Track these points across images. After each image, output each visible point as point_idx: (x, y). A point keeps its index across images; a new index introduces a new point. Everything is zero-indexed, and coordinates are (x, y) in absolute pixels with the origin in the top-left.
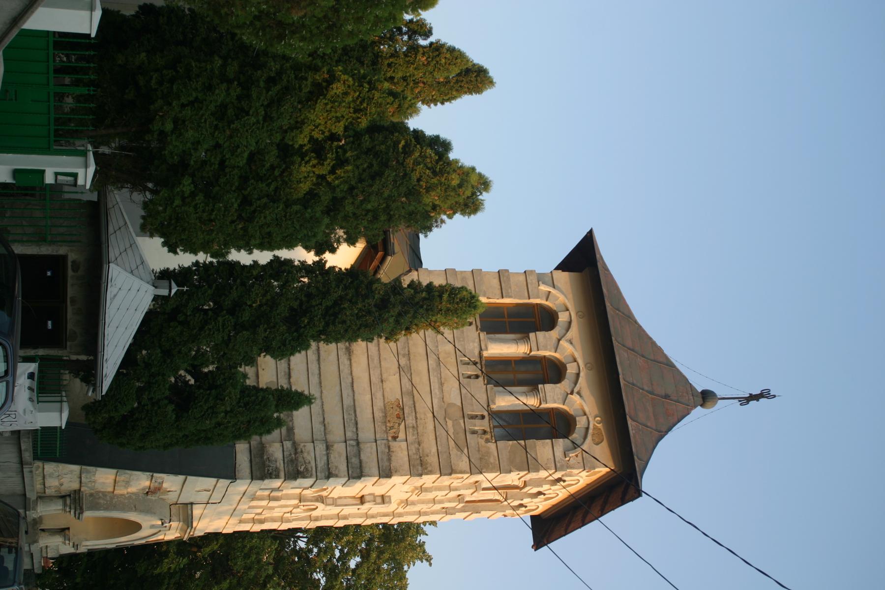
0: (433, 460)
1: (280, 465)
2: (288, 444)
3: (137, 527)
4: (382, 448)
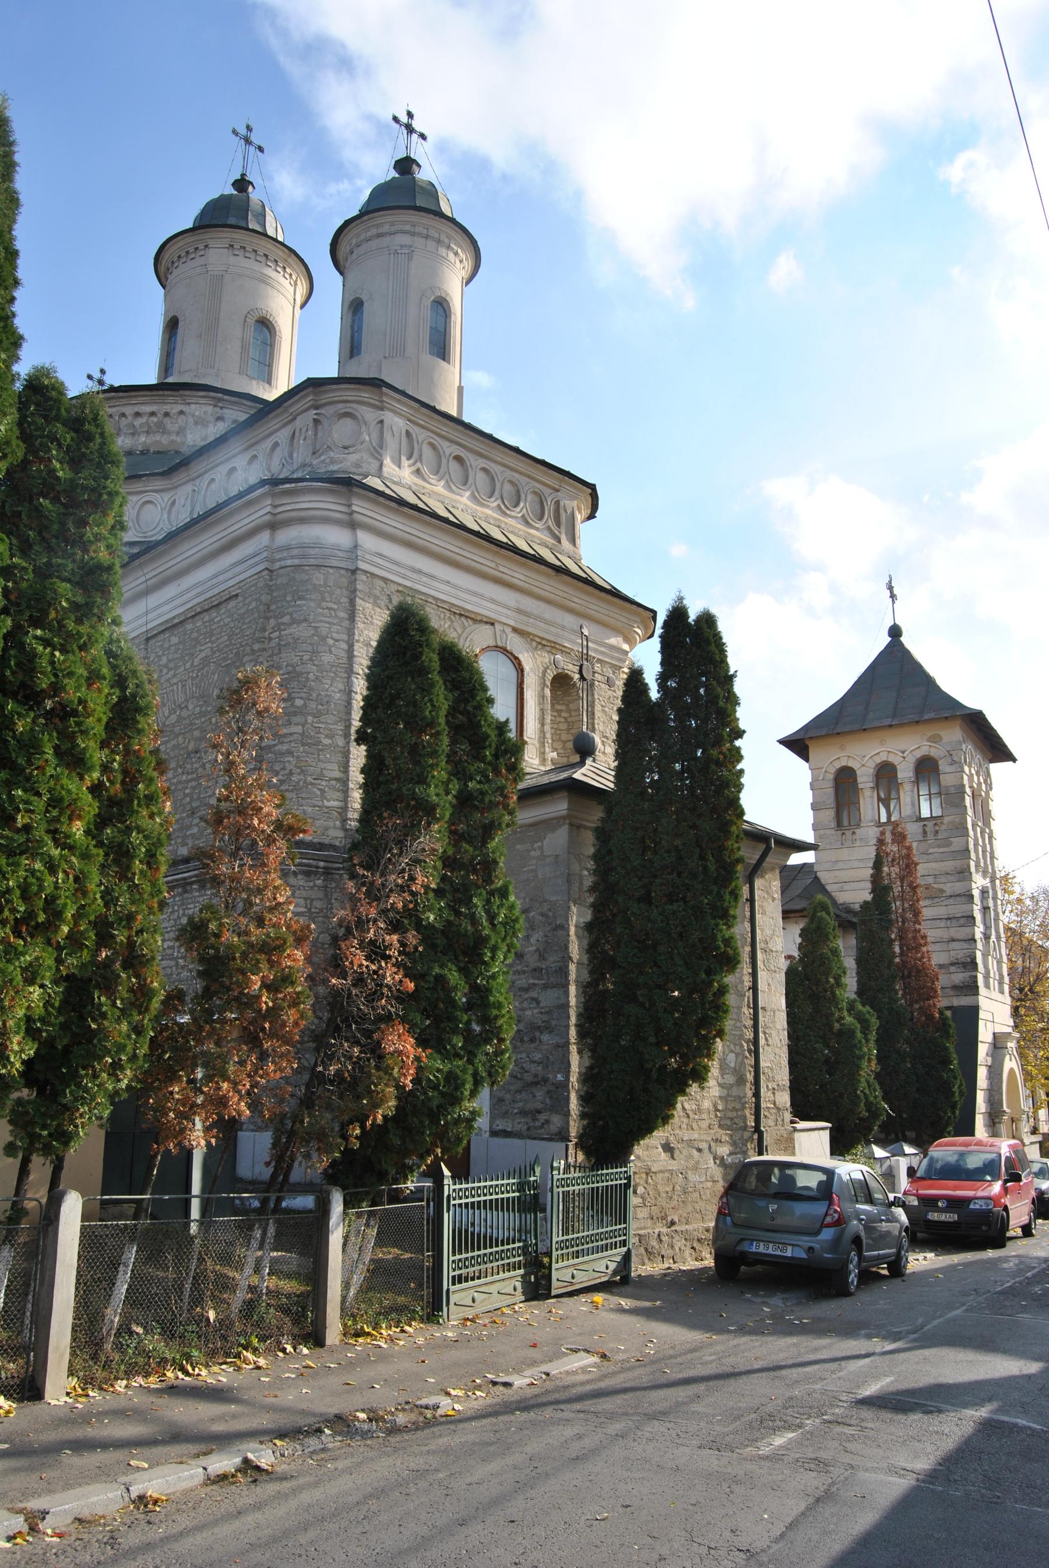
0: (958, 864)
1: (967, 974)
2: (952, 969)
3: (1012, 1070)
4: (951, 901)
